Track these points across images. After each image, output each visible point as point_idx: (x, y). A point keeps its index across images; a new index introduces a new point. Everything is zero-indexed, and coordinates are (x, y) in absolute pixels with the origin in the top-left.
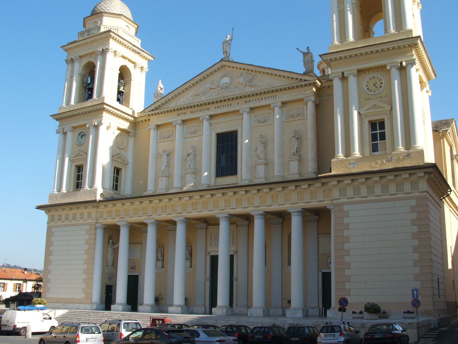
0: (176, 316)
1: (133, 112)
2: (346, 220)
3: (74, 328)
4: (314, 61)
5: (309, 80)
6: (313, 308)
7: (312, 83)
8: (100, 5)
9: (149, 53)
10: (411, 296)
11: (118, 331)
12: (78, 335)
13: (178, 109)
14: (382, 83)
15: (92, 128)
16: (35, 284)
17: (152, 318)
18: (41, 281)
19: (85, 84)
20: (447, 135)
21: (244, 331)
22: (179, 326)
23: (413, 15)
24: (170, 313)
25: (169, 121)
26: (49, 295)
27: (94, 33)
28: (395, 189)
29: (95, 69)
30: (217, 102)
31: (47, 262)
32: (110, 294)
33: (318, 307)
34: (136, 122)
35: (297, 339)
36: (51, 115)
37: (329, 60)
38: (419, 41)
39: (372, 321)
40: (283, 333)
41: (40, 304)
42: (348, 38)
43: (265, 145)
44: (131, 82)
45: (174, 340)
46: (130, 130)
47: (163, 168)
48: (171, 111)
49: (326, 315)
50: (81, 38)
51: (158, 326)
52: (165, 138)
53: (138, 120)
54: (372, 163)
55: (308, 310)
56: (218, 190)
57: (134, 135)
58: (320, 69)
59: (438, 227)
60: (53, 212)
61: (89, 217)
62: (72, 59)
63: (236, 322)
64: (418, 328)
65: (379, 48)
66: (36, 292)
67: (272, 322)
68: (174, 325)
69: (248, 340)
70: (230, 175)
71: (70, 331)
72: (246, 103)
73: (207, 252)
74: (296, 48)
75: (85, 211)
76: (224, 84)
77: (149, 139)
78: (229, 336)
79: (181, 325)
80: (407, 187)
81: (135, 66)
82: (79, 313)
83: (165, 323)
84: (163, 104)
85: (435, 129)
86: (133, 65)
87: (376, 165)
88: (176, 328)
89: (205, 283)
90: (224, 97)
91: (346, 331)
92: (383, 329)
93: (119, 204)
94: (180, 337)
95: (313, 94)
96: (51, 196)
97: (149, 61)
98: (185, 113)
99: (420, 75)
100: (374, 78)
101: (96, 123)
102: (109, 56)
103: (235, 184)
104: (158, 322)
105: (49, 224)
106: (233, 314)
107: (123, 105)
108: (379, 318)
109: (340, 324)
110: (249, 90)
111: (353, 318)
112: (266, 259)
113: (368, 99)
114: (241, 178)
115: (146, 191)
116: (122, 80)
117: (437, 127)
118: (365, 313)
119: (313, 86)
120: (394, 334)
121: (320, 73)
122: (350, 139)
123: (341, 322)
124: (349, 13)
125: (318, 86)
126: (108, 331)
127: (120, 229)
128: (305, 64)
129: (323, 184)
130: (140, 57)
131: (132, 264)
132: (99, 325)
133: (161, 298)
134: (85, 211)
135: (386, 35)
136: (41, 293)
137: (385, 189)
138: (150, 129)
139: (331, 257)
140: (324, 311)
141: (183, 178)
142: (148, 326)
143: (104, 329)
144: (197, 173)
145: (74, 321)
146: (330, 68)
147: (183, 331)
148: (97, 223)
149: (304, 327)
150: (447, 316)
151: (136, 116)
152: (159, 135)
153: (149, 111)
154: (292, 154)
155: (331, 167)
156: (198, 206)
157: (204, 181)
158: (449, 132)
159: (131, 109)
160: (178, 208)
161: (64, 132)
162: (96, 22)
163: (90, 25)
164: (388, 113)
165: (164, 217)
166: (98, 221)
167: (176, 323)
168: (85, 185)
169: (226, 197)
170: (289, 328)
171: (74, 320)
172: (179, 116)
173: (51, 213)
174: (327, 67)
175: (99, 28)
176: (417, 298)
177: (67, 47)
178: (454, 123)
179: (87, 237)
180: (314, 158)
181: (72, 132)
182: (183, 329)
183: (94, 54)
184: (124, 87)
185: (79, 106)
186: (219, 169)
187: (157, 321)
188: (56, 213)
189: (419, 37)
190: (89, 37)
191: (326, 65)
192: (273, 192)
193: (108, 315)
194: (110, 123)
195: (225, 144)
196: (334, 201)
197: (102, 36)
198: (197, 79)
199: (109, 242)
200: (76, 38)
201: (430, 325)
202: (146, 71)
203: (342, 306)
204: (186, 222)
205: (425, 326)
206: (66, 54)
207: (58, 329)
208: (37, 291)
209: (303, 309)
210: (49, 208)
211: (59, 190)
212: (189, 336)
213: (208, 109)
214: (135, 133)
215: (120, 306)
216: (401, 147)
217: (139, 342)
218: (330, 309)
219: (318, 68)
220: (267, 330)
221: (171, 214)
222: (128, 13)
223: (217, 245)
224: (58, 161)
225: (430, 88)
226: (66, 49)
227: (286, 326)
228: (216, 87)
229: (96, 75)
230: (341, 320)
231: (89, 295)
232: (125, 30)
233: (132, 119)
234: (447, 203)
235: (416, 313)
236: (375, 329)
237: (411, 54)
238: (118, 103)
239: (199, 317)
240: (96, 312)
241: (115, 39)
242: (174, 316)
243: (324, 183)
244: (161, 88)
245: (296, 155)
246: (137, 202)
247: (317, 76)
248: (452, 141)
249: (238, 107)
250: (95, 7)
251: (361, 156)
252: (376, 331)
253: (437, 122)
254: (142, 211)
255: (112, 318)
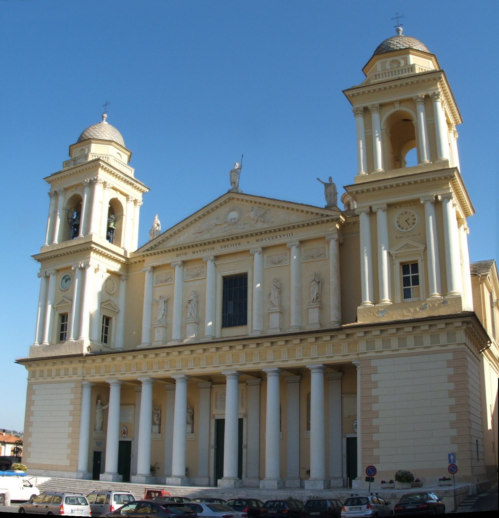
0: (175, 488)
1: (126, 252)
2: (374, 378)
3: (58, 498)
4: (337, 193)
5: (331, 216)
6: (336, 478)
7: (335, 219)
8: (88, 131)
9: (143, 184)
10: (448, 461)
11: (107, 503)
12: (62, 505)
13: (177, 249)
14: (415, 219)
15: (77, 271)
16: (15, 448)
17: (147, 490)
18: (21, 444)
19: (70, 220)
20: (486, 281)
21: (255, 505)
22: (178, 499)
23: (449, 144)
24: (168, 485)
25: (166, 262)
26: (29, 460)
27: (81, 163)
28: (429, 341)
29: (81, 203)
30: (223, 240)
31: (28, 423)
32: (99, 462)
33: (342, 477)
34: (128, 263)
35: (318, 513)
36: (32, 255)
37: (354, 193)
38: (456, 174)
39: (404, 491)
40: (301, 507)
41: (19, 469)
42: (377, 167)
43: (280, 290)
44: (123, 217)
45: (173, 515)
46: (121, 273)
47: (160, 317)
48: (169, 251)
49: (351, 485)
50: (66, 168)
51: (154, 499)
52: (162, 282)
53: (131, 261)
54: (404, 311)
55: (330, 481)
56: (224, 343)
57: (126, 278)
58: (345, 203)
59: (477, 384)
60: (34, 368)
61: (75, 373)
62: (56, 192)
63: (245, 496)
64: (455, 496)
65: (412, 180)
66: (15, 456)
67: (289, 494)
68: (172, 499)
69: (260, 516)
70: (239, 325)
71: (53, 501)
72: (258, 243)
73: (211, 416)
74: (316, 178)
75: (70, 366)
76: (231, 219)
77: (144, 283)
78: (237, 510)
79: (181, 498)
80: (443, 339)
81: (128, 199)
82: (63, 482)
83: (162, 496)
84: (159, 243)
85: (473, 273)
86: (125, 198)
87: (409, 314)
88: (175, 501)
89: (209, 451)
90: (232, 235)
91: (374, 502)
92: (416, 499)
93: (108, 359)
94: (179, 512)
95: (336, 232)
96: (32, 349)
97: (144, 193)
98: (186, 254)
99: (457, 210)
100: (406, 213)
101: (82, 265)
102: (98, 188)
103: (244, 336)
104: (153, 495)
105: (30, 381)
106: (243, 487)
107: (114, 244)
108: (412, 487)
109: (368, 496)
110: (260, 226)
111: (382, 488)
112: (281, 423)
113: (399, 238)
114: (252, 329)
115: (139, 344)
116: (113, 215)
117: (476, 271)
118: (396, 482)
119: (336, 222)
120: (428, 504)
121: (344, 207)
122: (378, 284)
123: (369, 494)
124: (378, 139)
125: (342, 222)
126: (96, 503)
127: (110, 388)
128: (326, 197)
129: (348, 335)
130: (133, 189)
131: (124, 429)
132: (86, 495)
133: (157, 467)
134: (71, 367)
135: (420, 165)
136: (20, 458)
137: (418, 341)
138: (145, 272)
139: (356, 420)
140: (349, 482)
141: (183, 328)
142: (142, 499)
143: (91, 501)
144: (199, 323)
145: (58, 490)
146: (356, 202)
147: (183, 505)
148: (83, 380)
149: (325, 500)
150: (487, 481)
151: (128, 256)
152: (155, 278)
153: (144, 251)
154: (312, 300)
155: (357, 316)
156: (201, 361)
157: (207, 333)
158: (489, 277)
159: (123, 248)
160: (177, 364)
161: (46, 276)
162: (84, 150)
163: (76, 153)
164: (422, 253)
165: (161, 374)
166: (85, 378)
167: (175, 496)
168: (70, 336)
169: (234, 351)
170: (309, 502)
171: (57, 489)
172: (178, 257)
173: (32, 369)
174: (353, 200)
175: (86, 156)
176: (454, 464)
177: (49, 180)
178: (494, 264)
179: (72, 396)
180: (337, 306)
181: (55, 276)
182: (183, 502)
183: (81, 185)
184: (114, 224)
185: (64, 245)
186: (226, 317)
187: (153, 494)
188: (37, 369)
189: (456, 168)
190: (75, 166)
191: (351, 197)
192: (289, 345)
193: (96, 485)
194: (98, 265)
195: (233, 288)
196: (360, 356)
197: (90, 165)
198: (200, 214)
199: (97, 403)
200: (61, 169)
201: (468, 492)
202: (140, 204)
203: (369, 476)
204: (187, 380)
205: (463, 493)
206: (49, 186)
207: (40, 498)
208: (16, 455)
209: (323, 480)
210: (30, 363)
211: (41, 342)
212: (190, 511)
213: (213, 249)
214: (127, 276)
215: (109, 475)
216: (436, 293)
217: (132, 516)
218: (356, 479)
219: (343, 201)
220: (282, 504)
221: (169, 370)
222: (119, 139)
223: (223, 407)
224: (40, 309)
225: (468, 226)
226: (50, 181)
227: (305, 500)
228: (223, 223)
229: (83, 210)
230: (368, 491)
231: (74, 462)
232: (116, 158)
233: (124, 260)
234: (487, 356)
235: (452, 480)
236: (407, 499)
237: (447, 187)
238: (108, 241)
239: (202, 489)
240: (82, 481)
241: (105, 169)
242: (172, 488)
243: (349, 334)
244: (157, 224)
245: (316, 302)
246: (129, 357)
247: (340, 210)
248: (492, 287)
249: (248, 247)
250: (83, 133)
251: (392, 303)
252: (408, 502)
253: (476, 265)
254: (135, 367)
255: (101, 489)
